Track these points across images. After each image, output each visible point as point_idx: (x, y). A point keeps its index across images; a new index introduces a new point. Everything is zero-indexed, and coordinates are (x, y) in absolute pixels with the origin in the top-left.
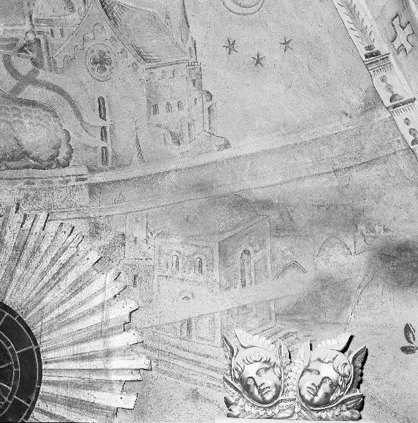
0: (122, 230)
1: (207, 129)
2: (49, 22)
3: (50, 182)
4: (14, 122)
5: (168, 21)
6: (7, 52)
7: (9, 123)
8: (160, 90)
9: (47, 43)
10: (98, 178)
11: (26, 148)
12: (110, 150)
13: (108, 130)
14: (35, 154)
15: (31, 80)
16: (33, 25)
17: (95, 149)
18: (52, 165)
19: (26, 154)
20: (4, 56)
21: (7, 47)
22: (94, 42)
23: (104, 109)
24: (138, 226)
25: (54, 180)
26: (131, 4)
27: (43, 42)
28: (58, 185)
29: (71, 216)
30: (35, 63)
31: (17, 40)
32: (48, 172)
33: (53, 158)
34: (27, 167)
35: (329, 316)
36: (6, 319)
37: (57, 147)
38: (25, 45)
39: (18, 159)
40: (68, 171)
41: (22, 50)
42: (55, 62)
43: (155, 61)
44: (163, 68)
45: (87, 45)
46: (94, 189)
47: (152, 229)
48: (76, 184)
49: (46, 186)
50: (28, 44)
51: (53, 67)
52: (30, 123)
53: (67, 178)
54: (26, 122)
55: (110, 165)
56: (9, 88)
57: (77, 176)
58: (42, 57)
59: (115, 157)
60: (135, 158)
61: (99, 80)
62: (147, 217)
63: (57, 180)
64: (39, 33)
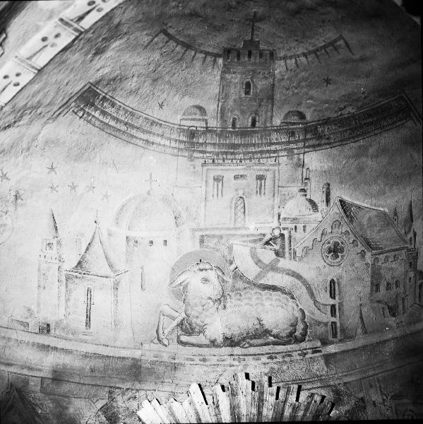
5: (396, 217)
6: (252, 245)
9: (290, 237)
11: (267, 327)
12: (338, 325)
13: (337, 307)
14: (275, 331)
17: (326, 324)
18: (291, 340)
19: (267, 332)
22: (331, 236)
23: (335, 290)
25: (294, 354)
27: (287, 236)
30: (277, 254)
31: (264, 235)
33: (291, 334)
34: (267, 344)
35: (375, 188)
38: (271, 239)
40: (303, 345)
41: (267, 243)
43: (381, 248)
48: (312, 356)
49: (287, 359)
53: (305, 351)
55: (339, 337)
57: (312, 348)
59: (343, 330)
60: (359, 331)
64: (284, 229)
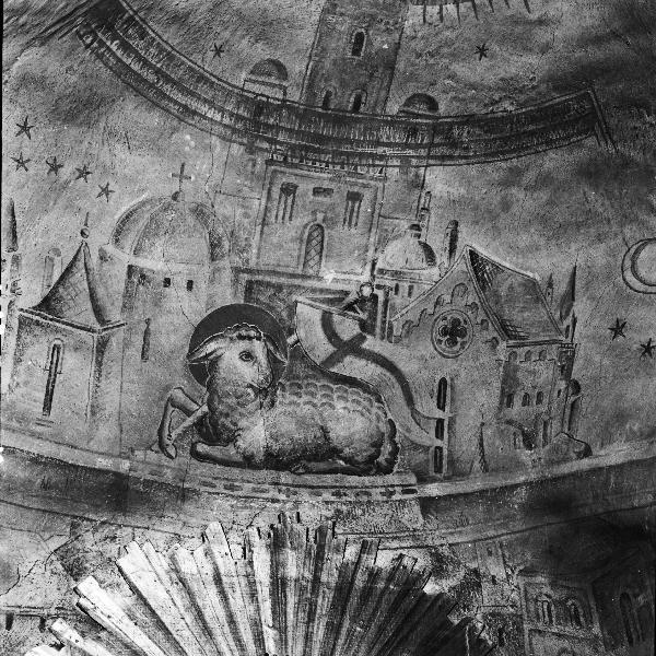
0: (473, 565)
1: (566, 431)
2: (397, 274)
3: (368, 494)
4: (323, 404)
5: (550, 290)
7: (314, 406)
8: (519, 375)
10: (433, 490)
11: (335, 443)
12: (445, 452)
13: (446, 423)
15: (354, 348)
16: (374, 277)
18: (371, 469)
19: (335, 452)
20: (325, 312)
21: (330, 302)
23: (445, 396)
24: (490, 560)
25: (373, 491)
26: (508, 265)
28: (380, 498)
29: (404, 545)
32: (367, 480)
33: (372, 459)
36: (465, 648)
37: (377, 445)
39: (323, 459)
41: (350, 307)
42: (391, 328)
43: (521, 338)
44: (528, 348)
45: (441, 310)
46: (427, 505)
47: (511, 564)
49: (365, 498)
50: (361, 301)
51: (388, 334)
52: (345, 408)
54: (339, 405)
56: (323, 357)
58: (375, 320)
60: (477, 465)
61: (444, 356)
62: (501, 547)
63: (378, 490)
64: (379, 287)
